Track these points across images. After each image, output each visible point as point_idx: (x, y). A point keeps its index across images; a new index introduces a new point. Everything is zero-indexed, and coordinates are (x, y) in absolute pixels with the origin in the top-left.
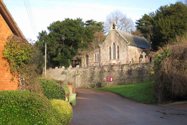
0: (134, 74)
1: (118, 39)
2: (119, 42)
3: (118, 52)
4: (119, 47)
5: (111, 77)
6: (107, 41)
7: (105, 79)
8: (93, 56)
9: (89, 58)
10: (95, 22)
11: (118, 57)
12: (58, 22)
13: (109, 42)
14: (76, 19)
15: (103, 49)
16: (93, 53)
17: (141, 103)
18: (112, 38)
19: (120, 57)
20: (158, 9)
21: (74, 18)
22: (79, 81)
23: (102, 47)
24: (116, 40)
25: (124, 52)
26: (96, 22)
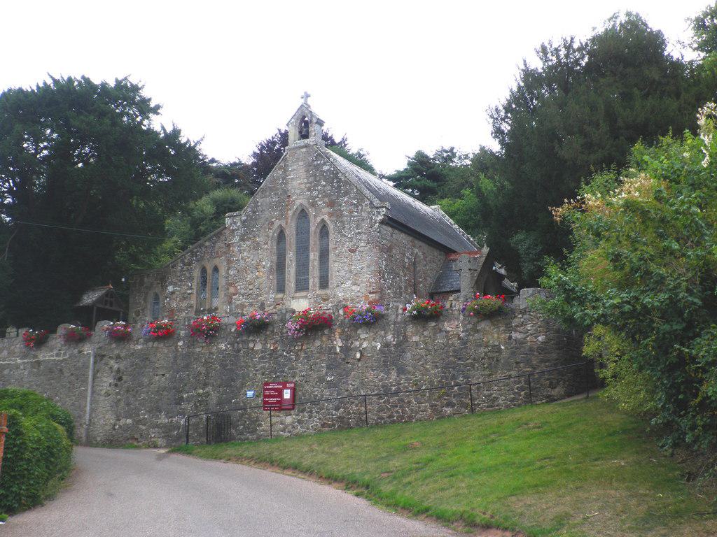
0: (414, 366)
1: (328, 188)
2: (331, 204)
3: (324, 255)
4: (331, 227)
5: (285, 387)
6: (268, 200)
7: (250, 394)
8: (191, 279)
9: (170, 288)
10: (213, 161)
11: (324, 283)
12: (20, 90)
13: (278, 204)
14: (112, 84)
15: (242, 239)
16: (190, 264)
17: (596, 388)
18: (295, 183)
19: (333, 282)
20: (501, 108)
21: (103, 74)
22: (104, 404)
23: (242, 231)
24: (315, 193)
25: (356, 256)
26: (214, 165)
